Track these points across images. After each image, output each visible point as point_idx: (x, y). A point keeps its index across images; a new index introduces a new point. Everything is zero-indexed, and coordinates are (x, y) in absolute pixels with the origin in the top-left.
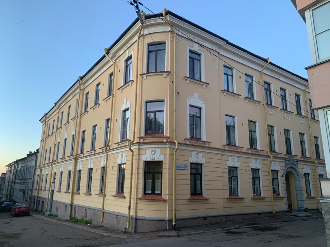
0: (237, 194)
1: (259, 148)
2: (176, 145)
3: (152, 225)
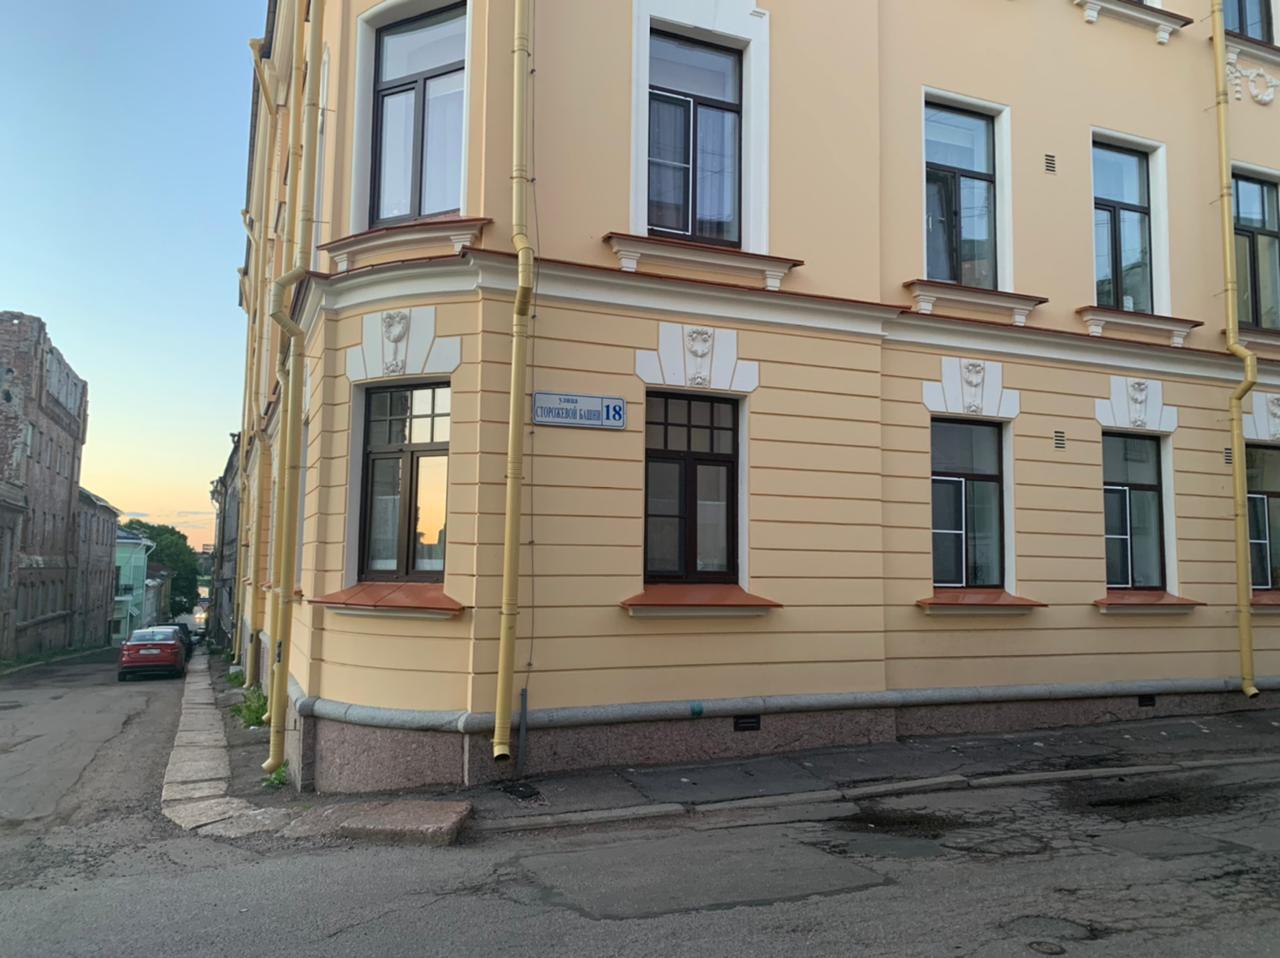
0: (996, 581)
1: (1163, 308)
2: (520, 275)
3: (383, 755)
